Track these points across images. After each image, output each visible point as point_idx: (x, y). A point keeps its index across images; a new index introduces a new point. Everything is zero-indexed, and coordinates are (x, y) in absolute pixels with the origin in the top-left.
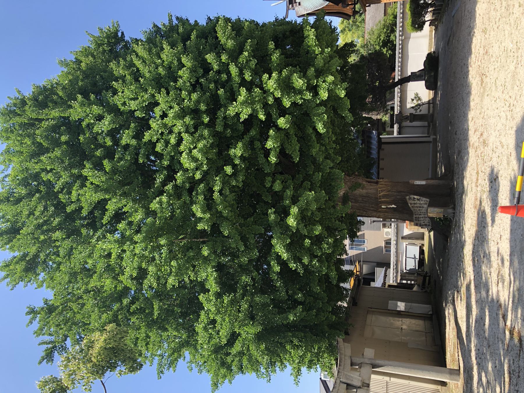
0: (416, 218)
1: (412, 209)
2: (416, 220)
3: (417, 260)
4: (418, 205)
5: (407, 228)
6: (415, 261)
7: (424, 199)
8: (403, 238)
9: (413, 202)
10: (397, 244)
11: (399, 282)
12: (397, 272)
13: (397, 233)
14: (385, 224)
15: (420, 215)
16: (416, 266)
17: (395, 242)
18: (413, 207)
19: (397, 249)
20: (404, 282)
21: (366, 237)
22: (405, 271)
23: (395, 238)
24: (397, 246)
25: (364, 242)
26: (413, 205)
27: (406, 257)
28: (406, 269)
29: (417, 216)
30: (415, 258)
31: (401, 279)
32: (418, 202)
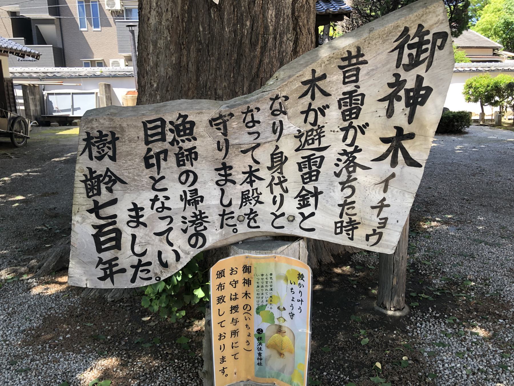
0: (185, 128)
1: (287, 81)
2: (154, 130)
3: (70, 114)
4: (334, 144)
5: (128, 93)
6: (69, 110)
7: (401, 205)
8: (108, 87)
9: (373, 85)
10: (95, 77)
11: (14, 82)
12: (38, 78)
13: (115, 76)
14: (131, 60)
15: (225, 171)
16: (58, 111)
17: (98, 73)
18: (313, 85)
19: (86, 77)
20: (19, 92)
21: (105, 29)
22: (45, 93)
23: (106, 74)
24: (91, 77)
25: (96, 26)
26: (336, 85)
27: (73, 94)
28: (49, 94)
29: (205, 142)
30: (74, 109)
31: (24, 87)
32: (370, 146)
